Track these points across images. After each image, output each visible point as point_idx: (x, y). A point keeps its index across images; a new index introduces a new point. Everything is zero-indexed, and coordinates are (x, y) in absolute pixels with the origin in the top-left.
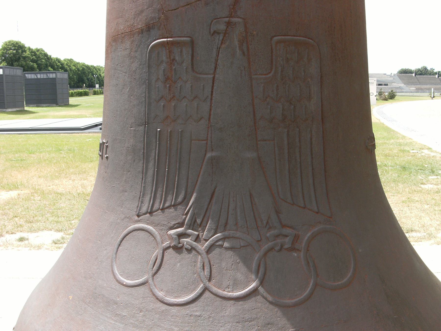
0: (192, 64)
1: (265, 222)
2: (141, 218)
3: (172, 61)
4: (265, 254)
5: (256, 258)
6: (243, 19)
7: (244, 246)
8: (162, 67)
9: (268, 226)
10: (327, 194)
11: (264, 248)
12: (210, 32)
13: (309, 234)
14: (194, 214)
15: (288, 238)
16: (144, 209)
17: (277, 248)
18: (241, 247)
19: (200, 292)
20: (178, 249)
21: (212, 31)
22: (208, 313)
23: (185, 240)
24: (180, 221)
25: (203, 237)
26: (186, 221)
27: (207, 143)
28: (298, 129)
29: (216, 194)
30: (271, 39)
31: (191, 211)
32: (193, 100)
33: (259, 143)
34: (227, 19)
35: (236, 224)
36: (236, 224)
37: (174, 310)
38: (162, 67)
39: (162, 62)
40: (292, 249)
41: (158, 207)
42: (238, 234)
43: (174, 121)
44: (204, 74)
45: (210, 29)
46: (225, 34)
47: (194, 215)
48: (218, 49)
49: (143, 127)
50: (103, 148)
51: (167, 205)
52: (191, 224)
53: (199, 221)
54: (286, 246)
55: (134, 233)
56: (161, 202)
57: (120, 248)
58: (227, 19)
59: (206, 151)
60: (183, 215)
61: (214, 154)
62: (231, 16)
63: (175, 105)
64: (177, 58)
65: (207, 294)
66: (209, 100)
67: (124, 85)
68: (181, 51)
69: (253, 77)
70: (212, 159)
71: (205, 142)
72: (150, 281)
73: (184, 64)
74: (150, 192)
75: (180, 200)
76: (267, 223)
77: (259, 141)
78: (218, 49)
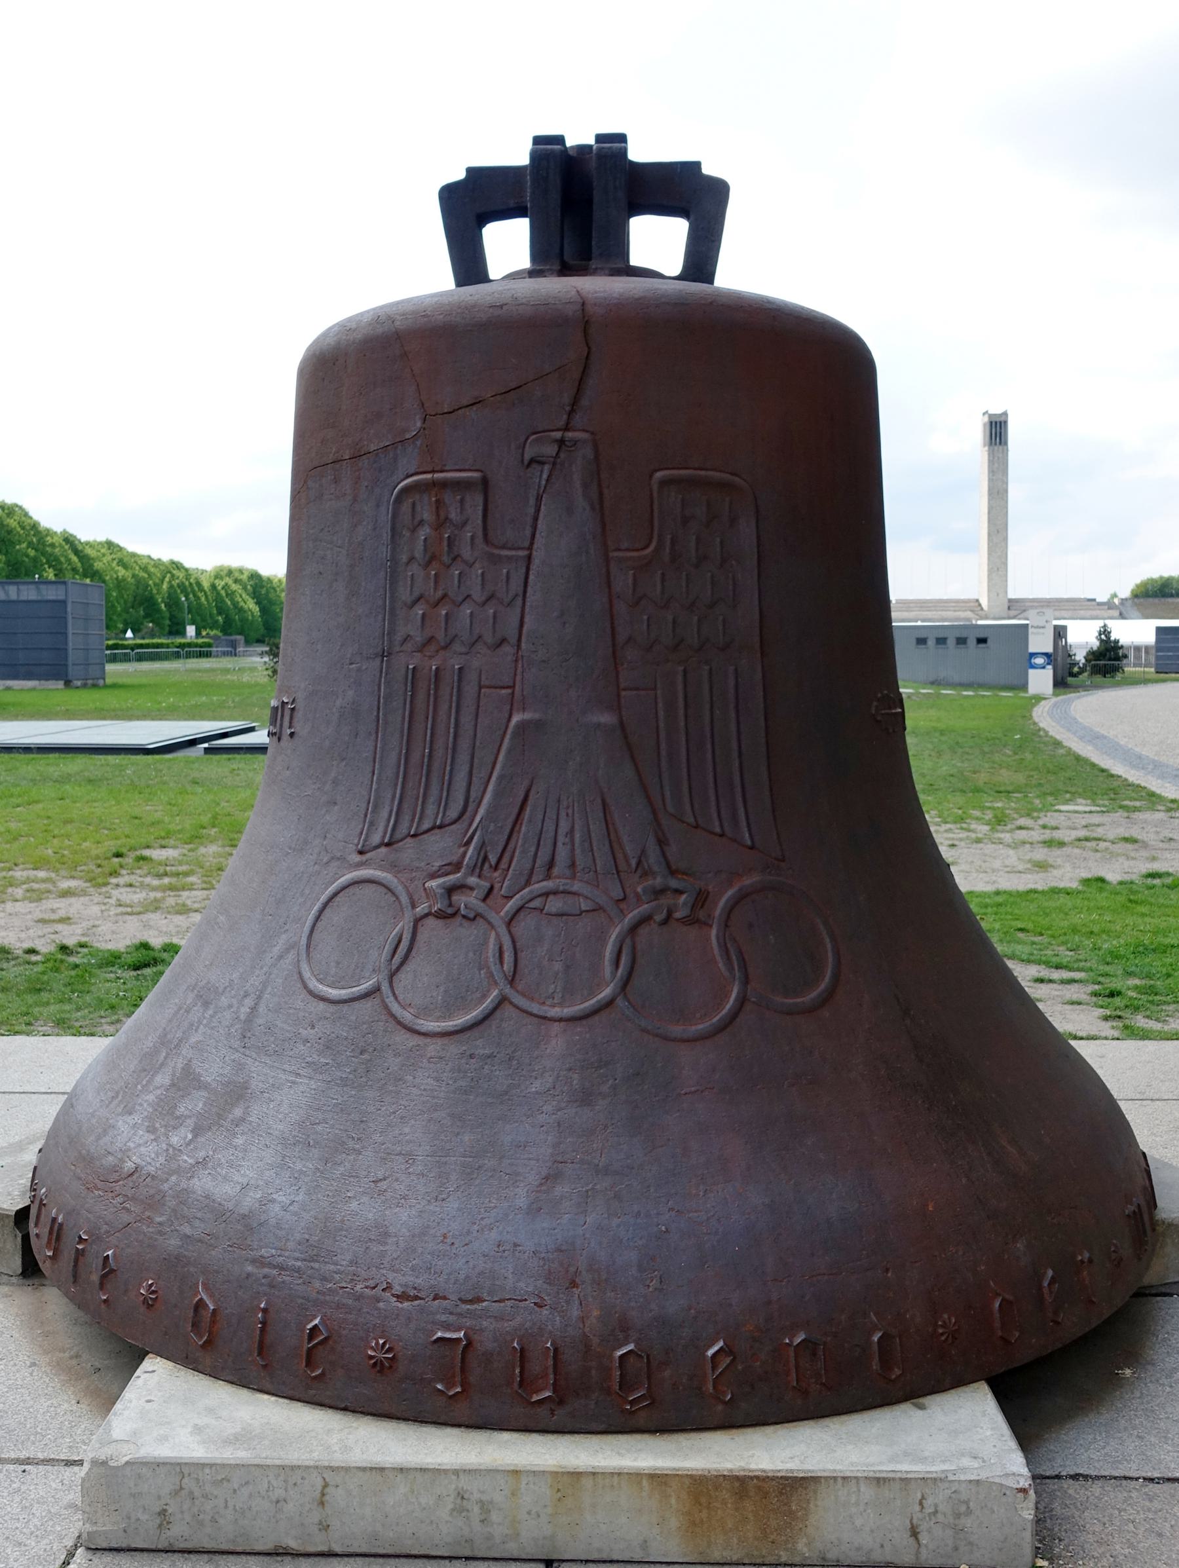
0: (485, 529)
1: (633, 862)
2: (368, 856)
3: (440, 524)
4: (633, 929)
5: (613, 937)
6: (592, 433)
7: (587, 911)
8: (424, 532)
9: (639, 871)
10: (774, 811)
11: (631, 915)
12: (522, 461)
13: (730, 893)
14: (484, 843)
15: (684, 897)
16: (376, 839)
17: (658, 918)
18: (582, 912)
19: (491, 1007)
20: (447, 915)
21: (527, 457)
22: (509, 1051)
23: (461, 899)
24: (455, 858)
25: (502, 892)
26: (467, 859)
27: (513, 693)
28: (707, 668)
29: (530, 802)
30: (651, 476)
31: (476, 837)
32: (484, 603)
33: (623, 693)
34: (558, 435)
35: (573, 865)
36: (573, 865)
37: (433, 1047)
38: (424, 532)
39: (421, 522)
40: (691, 920)
41: (405, 831)
42: (577, 886)
43: (445, 647)
44: (510, 549)
45: (523, 455)
46: (554, 464)
47: (483, 845)
48: (539, 499)
49: (378, 660)
50: (282, 716)
51: (426, 825)
52: (475, 865)
53: (493, 859)
54: (678, 915)
55: (351, 890)
56: (413, 820)
57: (319, 924)
58: (558, 435)
59: (511, 710)
60: (460, 846)
61: (527, 716)
62: (567, 428)
63: (447, 614)
64: (453, 516)
65: (508, 1011)
66: (519, 601)
67: (337, 574)
68: (462, 501)
69: (611, 554)
70: (523, 726)
71: (509, 691)
72: (385, 987)
73: (468, 528)
74: (388, 802)
75: (453, 813)
76: (639, 863)
77: (624, 689)
78: (539, 499)
